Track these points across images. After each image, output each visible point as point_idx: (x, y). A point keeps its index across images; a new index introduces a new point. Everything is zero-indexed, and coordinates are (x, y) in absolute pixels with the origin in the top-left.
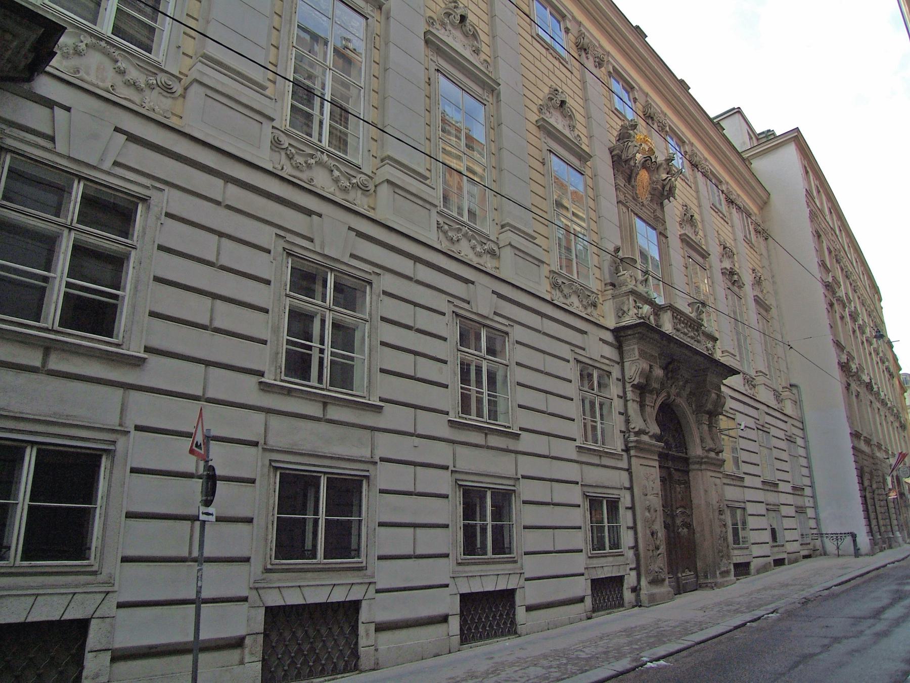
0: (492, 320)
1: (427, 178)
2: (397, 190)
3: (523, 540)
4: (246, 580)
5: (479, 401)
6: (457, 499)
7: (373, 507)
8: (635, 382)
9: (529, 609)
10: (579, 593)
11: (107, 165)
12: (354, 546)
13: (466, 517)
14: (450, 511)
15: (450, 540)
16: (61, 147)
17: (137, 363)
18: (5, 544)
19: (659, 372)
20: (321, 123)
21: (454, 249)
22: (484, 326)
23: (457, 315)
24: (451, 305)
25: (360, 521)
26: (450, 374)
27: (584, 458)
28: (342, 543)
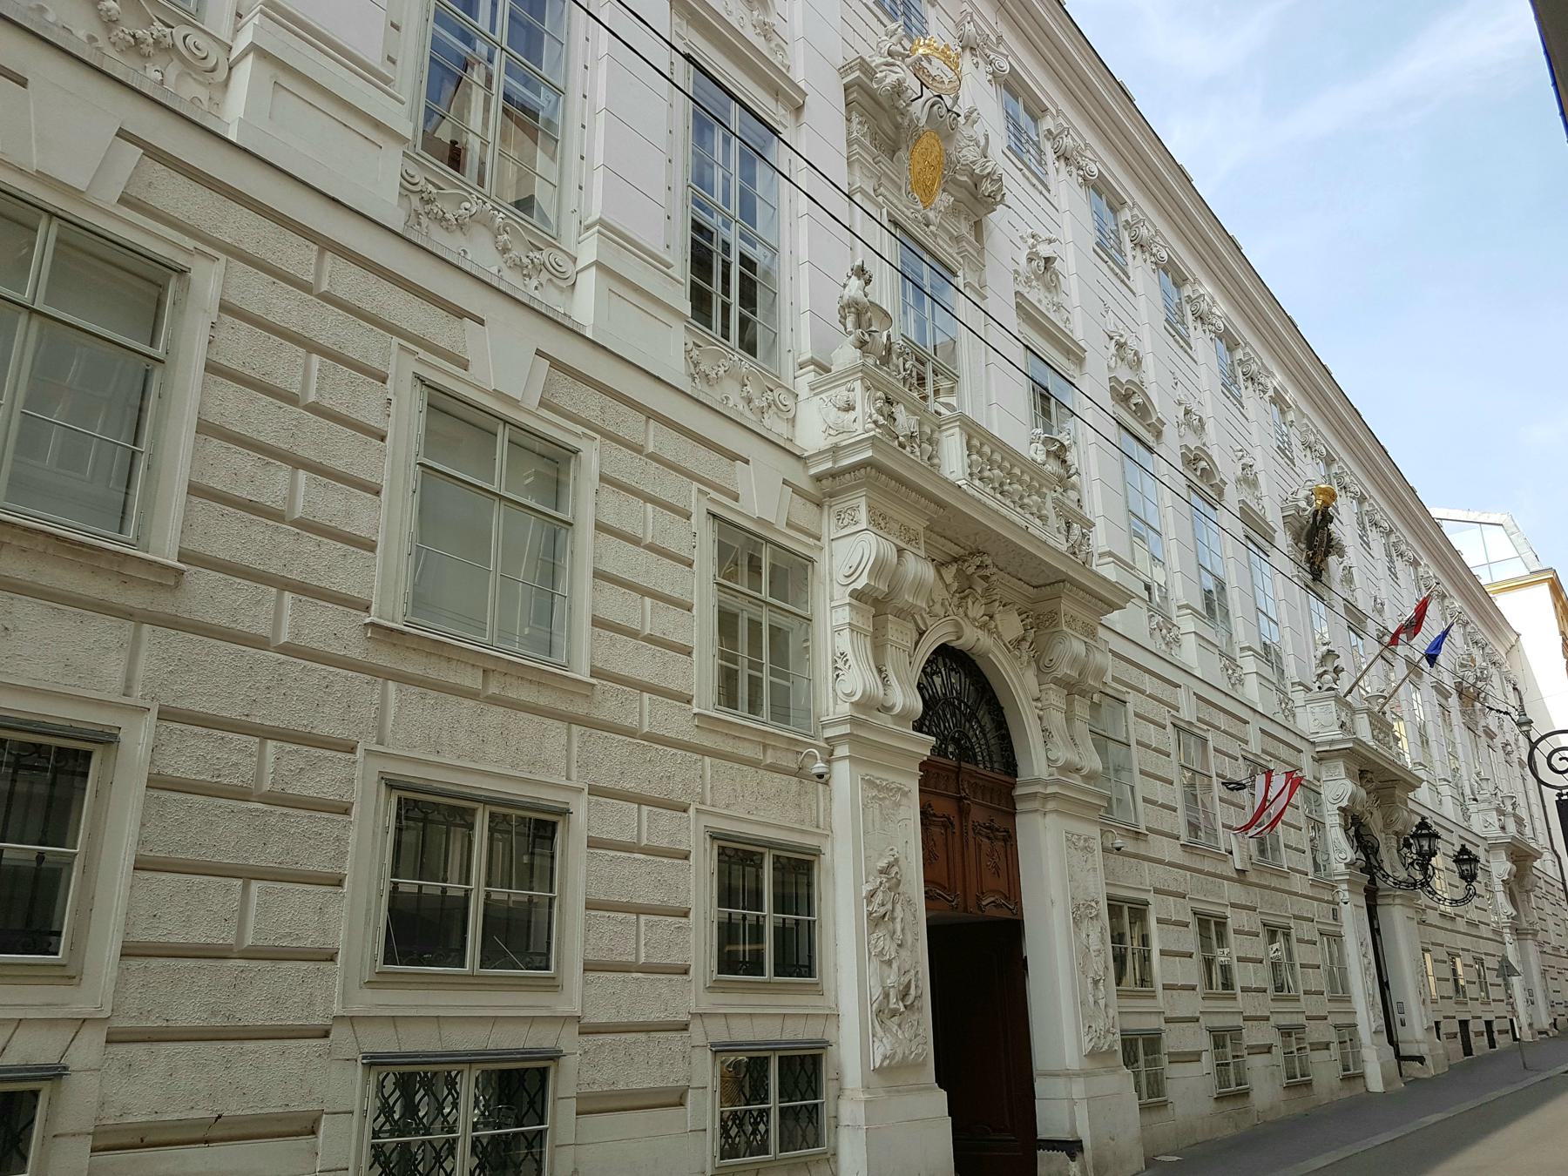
0: (538, 417)
1: (387, 81)
2: (285, 81)
3: (574, 937)
4: (342, 1010)
5: (755, 683)
6: (1194, 927)
7: (578, 872)
8: (859, 585)
9: (677, 1099)
10: (672, 1078)
11: (109, 195)
12: (804, 961)
13: (727, 896)
14: (698, 885)
15: (698, 942)
16: (472, 374)
17: (582, 690)
18: (55, 928)
19: (918, 568)
20: (726, 308)
21: (711, 396)
22: (768, 541)
23: (714, 516)
24: (704, 499)
25: (551, 900)
26: (701, 631)
27: (708, 741)
28: (520, 940)
